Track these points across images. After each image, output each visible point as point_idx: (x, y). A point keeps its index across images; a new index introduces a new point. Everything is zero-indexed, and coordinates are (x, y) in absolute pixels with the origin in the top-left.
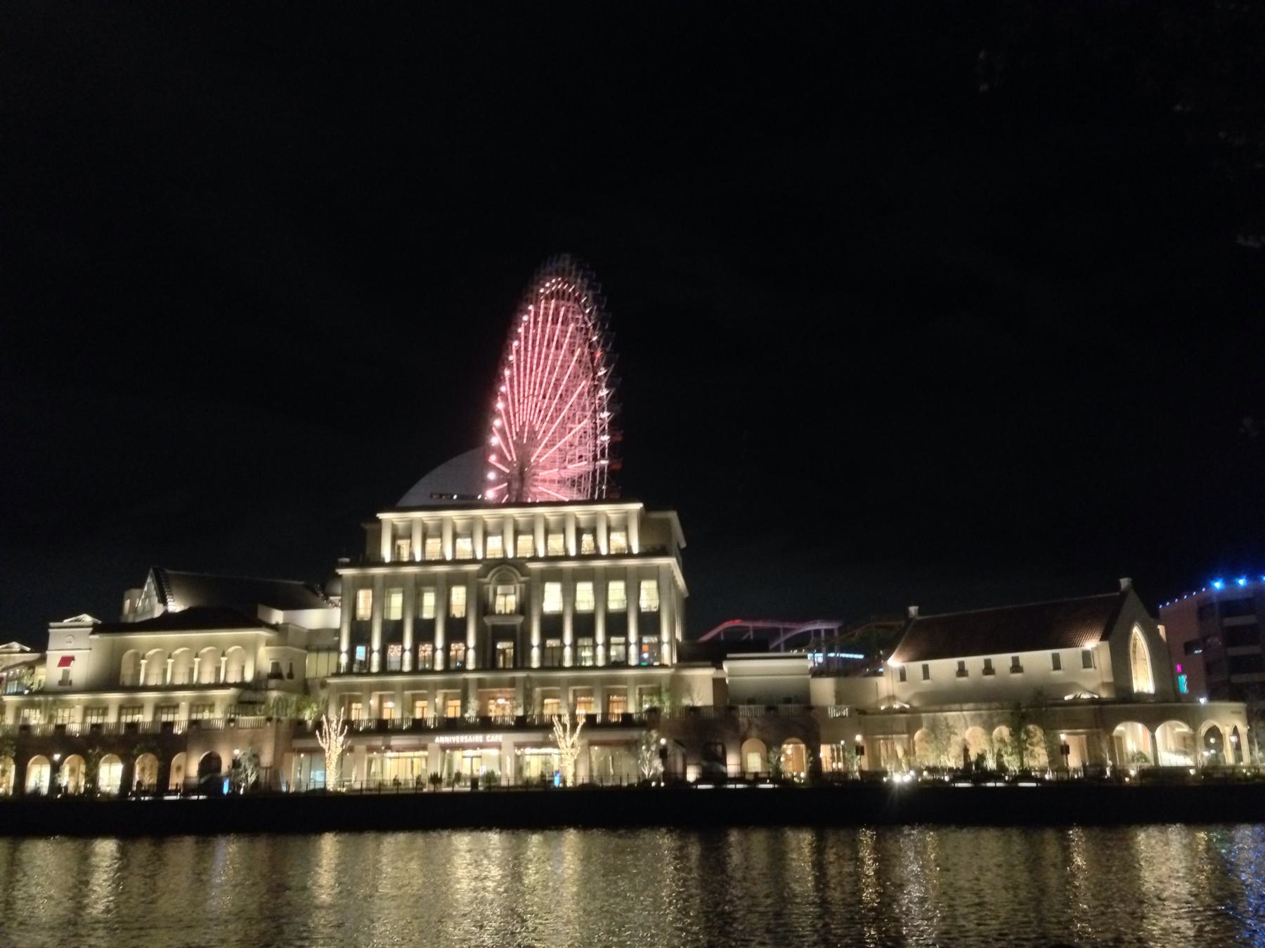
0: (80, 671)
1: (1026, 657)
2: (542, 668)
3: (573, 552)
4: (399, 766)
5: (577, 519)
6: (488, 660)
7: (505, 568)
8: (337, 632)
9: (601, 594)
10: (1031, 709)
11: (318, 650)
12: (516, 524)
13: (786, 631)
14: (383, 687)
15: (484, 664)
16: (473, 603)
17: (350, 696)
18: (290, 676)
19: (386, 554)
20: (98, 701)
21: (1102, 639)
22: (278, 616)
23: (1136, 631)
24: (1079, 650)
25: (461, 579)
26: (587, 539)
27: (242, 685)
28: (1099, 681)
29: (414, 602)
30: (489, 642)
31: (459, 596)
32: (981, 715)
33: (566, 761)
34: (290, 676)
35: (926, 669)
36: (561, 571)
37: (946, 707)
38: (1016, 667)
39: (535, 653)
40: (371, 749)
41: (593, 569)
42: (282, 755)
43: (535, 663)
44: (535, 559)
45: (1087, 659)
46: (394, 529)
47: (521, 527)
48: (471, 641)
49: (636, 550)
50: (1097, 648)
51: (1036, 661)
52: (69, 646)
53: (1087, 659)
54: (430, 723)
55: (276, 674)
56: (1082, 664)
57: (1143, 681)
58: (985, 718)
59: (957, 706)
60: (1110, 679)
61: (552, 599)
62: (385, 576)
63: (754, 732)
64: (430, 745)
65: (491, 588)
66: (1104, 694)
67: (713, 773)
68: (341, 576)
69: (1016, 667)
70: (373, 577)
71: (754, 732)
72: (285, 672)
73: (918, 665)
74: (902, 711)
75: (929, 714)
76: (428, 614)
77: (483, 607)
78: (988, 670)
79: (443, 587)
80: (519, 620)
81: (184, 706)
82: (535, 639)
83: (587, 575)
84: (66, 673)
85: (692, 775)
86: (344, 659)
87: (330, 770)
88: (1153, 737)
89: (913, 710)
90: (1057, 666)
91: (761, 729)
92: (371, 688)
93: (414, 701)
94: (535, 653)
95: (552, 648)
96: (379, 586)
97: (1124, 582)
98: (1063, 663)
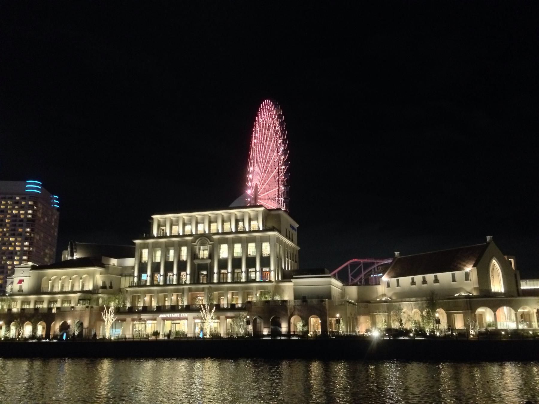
0: (26, 286)
1: (442, 276)
2: (219, 283)
3: (234, 230)
4: (148, 327)
5: (209, 217)
6: (195, 279)
7: (204, 238)
8: (133, 268)
9: (245, 249)
10: (432, 300)
11: (126, 276)
12: (210, 217)
13: (377, 263)
14: (149, 292)
15: (194, 280)
16: (190, 254)
17: (247, 292)
18: (111, 287)
19: (155, 232)
20: (27, 299)
21: (473, 267)
22: (114, 262)
23: (494, 261)
24: (464, 272)
25: (185, 244)
26: (241, 224)
27: (82, 292)
28: (473, 287)
29: (165, 254)
30: (197, 271)
31: (184, 251)
32: (418, 303)
33: (211, 325)
34: (111, 287)
35: (398, 281)
36: (227, 239)
37: (404, 300)
38: (436, 281)
39: (215, 276)
40: (133, 320)
41: (241, 238)
42: (95, 323)
43: (215, 281)
44: (217, 234)
45: (467, 276)
46: (159, 221)
47: (212, 220)
48: (188, 271)
49: (261, 229)
50: (471, 271)
51: (445, 277)
52: (22, 275)
53: (467, 276)
54: (167, 308)
55: (104, 287)
56: (464, 278)
57: (498, 285)
58: (420, 305)
59: (408, 299)
60: (477, 286)
61: (224, 252)
62: (153, 243)
63: (296, 312)
64: (158, 318)
65: (197, 247)
66: (475, 293)
67: (275, 332)
68: (135, 243)
69: (436, 281)
70: (148, 243)
71: (296, 312)
72: (108, 285)
73: (395, 279)
74: (386, 301)
75: (394, 303)
76: (171, 259)
77: (194, 256)
78: (424, 282)
79: (178, 247)
80: (209, 261)
81: (59, 301)
82: (216, 270)
83: (239, 241)
84: (21, 287)
85: (265, 332)
86: (136, 279)
87: (110, 330)
88: (495, 315)
89: (392, 301)
90: (454, 280)
91: (300, 311)
92: (145, 293)
93: (165, 298)
94: (215, 276)
95: (223, 273)
96: (150, 246)
97: (488, 238)
98: (457, 279)
